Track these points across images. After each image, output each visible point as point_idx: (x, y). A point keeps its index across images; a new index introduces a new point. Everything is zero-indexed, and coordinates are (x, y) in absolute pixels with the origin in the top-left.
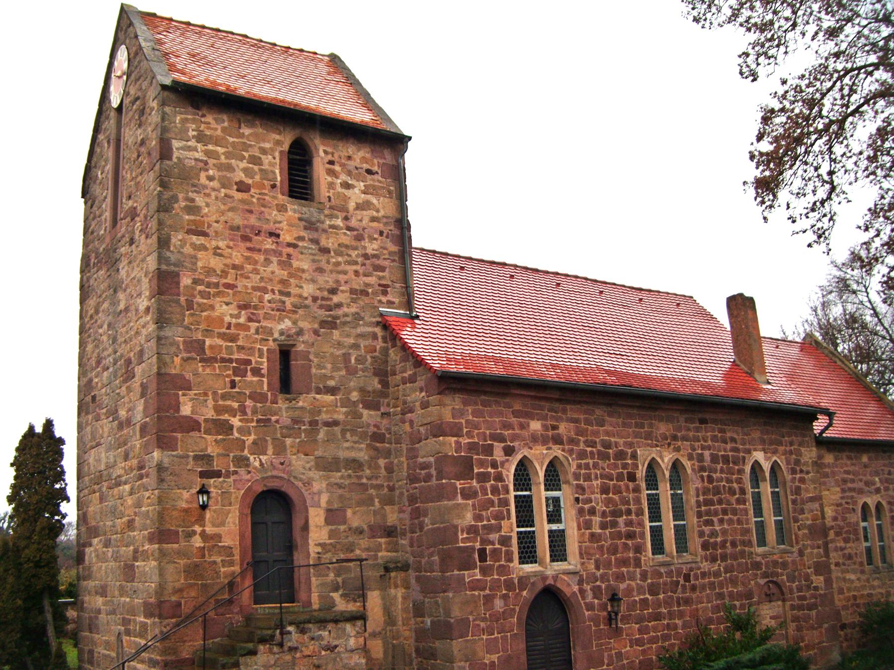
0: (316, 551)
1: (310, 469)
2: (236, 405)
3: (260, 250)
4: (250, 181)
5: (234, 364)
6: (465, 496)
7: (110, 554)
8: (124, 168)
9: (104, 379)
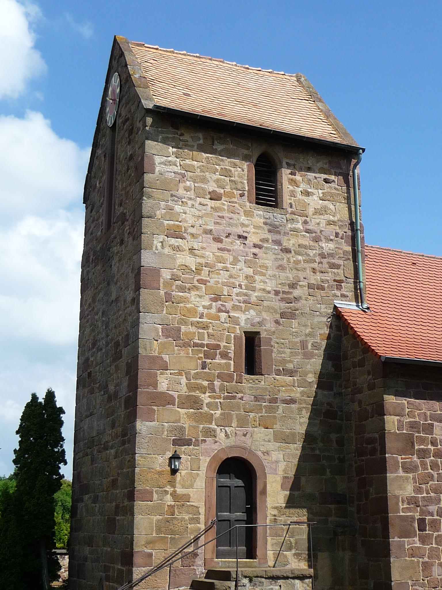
0: (273, 513)
1: (269, 441)
2: (206, 383)
3: (229, 251)
4: (222, 191)
5: (206, 349)
6: (406, 470)
7: (97, 509)
8: (117, 179)
9: (98, 358)
